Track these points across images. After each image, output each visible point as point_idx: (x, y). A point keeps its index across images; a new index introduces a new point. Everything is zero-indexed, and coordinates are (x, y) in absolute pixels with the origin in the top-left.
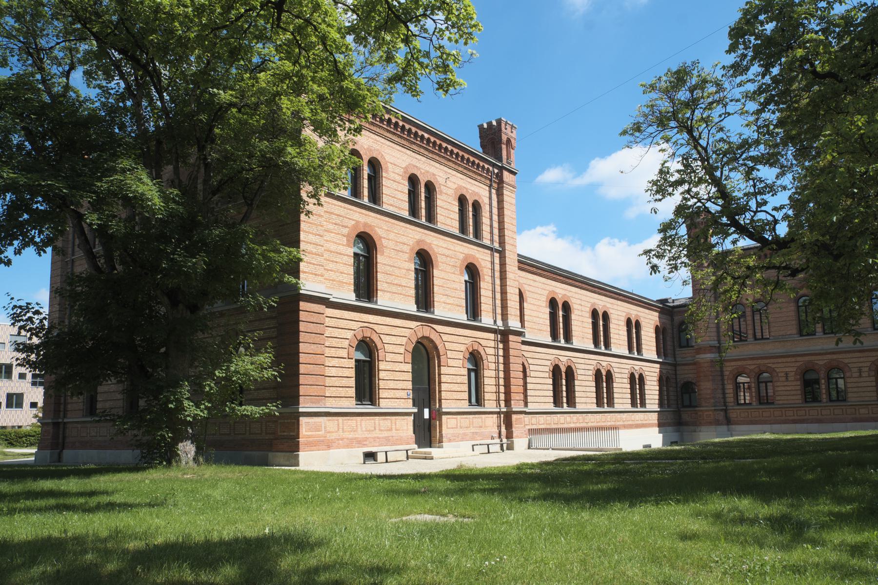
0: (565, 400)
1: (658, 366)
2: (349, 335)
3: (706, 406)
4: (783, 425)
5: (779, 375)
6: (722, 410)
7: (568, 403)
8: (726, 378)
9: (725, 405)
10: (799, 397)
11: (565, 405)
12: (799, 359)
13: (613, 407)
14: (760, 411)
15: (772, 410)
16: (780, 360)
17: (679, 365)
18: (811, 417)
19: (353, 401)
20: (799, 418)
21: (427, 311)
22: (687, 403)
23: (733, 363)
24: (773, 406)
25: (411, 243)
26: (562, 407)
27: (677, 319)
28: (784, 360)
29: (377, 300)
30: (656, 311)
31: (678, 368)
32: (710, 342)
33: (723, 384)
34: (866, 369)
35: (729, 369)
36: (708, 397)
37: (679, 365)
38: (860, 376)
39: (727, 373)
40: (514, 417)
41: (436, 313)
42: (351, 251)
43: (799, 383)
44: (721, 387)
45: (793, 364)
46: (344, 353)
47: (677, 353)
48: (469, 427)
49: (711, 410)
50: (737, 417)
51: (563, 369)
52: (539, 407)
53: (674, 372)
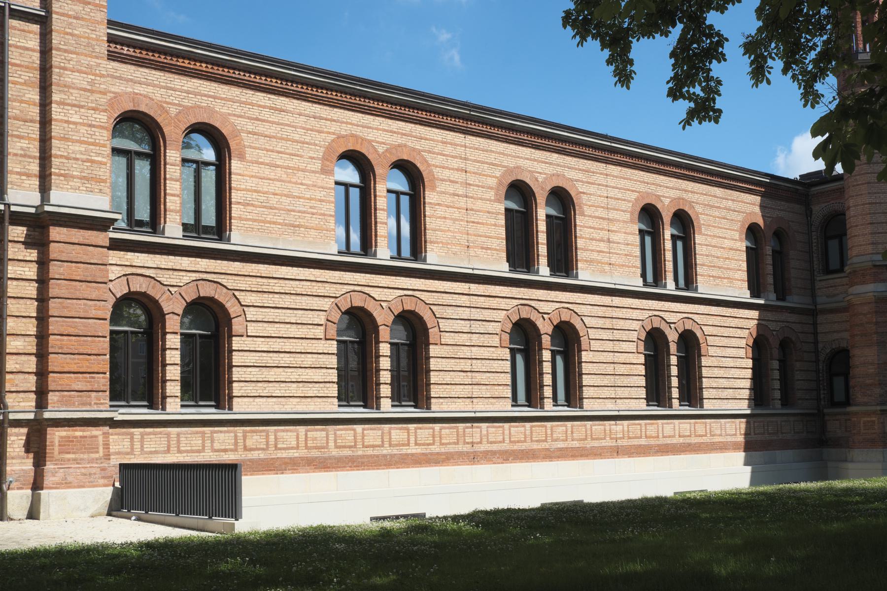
0: (675, 393)
1: (755, 314)
2: (501, 315)
3: (866, 404)
7: (681, 399)
11: (676, 403)
13: (702, 406)
17: (825, 311)
19: (105, 398)
21: (568, 275)
22: (839, 396)
25: (498, 174)
26: (671, 406)
27: (819, 210)
29: (577, 273)
30: (759, 196)
31: (821, 319)
36: (868, 382)
37: (825, 311)
40: (55, 436)
41: (379, 256)
42: (501, 208)
46: (319, 332)
47: (818, 285)
49: (874, 413)
51: (672, 336)
52: (277, 409)
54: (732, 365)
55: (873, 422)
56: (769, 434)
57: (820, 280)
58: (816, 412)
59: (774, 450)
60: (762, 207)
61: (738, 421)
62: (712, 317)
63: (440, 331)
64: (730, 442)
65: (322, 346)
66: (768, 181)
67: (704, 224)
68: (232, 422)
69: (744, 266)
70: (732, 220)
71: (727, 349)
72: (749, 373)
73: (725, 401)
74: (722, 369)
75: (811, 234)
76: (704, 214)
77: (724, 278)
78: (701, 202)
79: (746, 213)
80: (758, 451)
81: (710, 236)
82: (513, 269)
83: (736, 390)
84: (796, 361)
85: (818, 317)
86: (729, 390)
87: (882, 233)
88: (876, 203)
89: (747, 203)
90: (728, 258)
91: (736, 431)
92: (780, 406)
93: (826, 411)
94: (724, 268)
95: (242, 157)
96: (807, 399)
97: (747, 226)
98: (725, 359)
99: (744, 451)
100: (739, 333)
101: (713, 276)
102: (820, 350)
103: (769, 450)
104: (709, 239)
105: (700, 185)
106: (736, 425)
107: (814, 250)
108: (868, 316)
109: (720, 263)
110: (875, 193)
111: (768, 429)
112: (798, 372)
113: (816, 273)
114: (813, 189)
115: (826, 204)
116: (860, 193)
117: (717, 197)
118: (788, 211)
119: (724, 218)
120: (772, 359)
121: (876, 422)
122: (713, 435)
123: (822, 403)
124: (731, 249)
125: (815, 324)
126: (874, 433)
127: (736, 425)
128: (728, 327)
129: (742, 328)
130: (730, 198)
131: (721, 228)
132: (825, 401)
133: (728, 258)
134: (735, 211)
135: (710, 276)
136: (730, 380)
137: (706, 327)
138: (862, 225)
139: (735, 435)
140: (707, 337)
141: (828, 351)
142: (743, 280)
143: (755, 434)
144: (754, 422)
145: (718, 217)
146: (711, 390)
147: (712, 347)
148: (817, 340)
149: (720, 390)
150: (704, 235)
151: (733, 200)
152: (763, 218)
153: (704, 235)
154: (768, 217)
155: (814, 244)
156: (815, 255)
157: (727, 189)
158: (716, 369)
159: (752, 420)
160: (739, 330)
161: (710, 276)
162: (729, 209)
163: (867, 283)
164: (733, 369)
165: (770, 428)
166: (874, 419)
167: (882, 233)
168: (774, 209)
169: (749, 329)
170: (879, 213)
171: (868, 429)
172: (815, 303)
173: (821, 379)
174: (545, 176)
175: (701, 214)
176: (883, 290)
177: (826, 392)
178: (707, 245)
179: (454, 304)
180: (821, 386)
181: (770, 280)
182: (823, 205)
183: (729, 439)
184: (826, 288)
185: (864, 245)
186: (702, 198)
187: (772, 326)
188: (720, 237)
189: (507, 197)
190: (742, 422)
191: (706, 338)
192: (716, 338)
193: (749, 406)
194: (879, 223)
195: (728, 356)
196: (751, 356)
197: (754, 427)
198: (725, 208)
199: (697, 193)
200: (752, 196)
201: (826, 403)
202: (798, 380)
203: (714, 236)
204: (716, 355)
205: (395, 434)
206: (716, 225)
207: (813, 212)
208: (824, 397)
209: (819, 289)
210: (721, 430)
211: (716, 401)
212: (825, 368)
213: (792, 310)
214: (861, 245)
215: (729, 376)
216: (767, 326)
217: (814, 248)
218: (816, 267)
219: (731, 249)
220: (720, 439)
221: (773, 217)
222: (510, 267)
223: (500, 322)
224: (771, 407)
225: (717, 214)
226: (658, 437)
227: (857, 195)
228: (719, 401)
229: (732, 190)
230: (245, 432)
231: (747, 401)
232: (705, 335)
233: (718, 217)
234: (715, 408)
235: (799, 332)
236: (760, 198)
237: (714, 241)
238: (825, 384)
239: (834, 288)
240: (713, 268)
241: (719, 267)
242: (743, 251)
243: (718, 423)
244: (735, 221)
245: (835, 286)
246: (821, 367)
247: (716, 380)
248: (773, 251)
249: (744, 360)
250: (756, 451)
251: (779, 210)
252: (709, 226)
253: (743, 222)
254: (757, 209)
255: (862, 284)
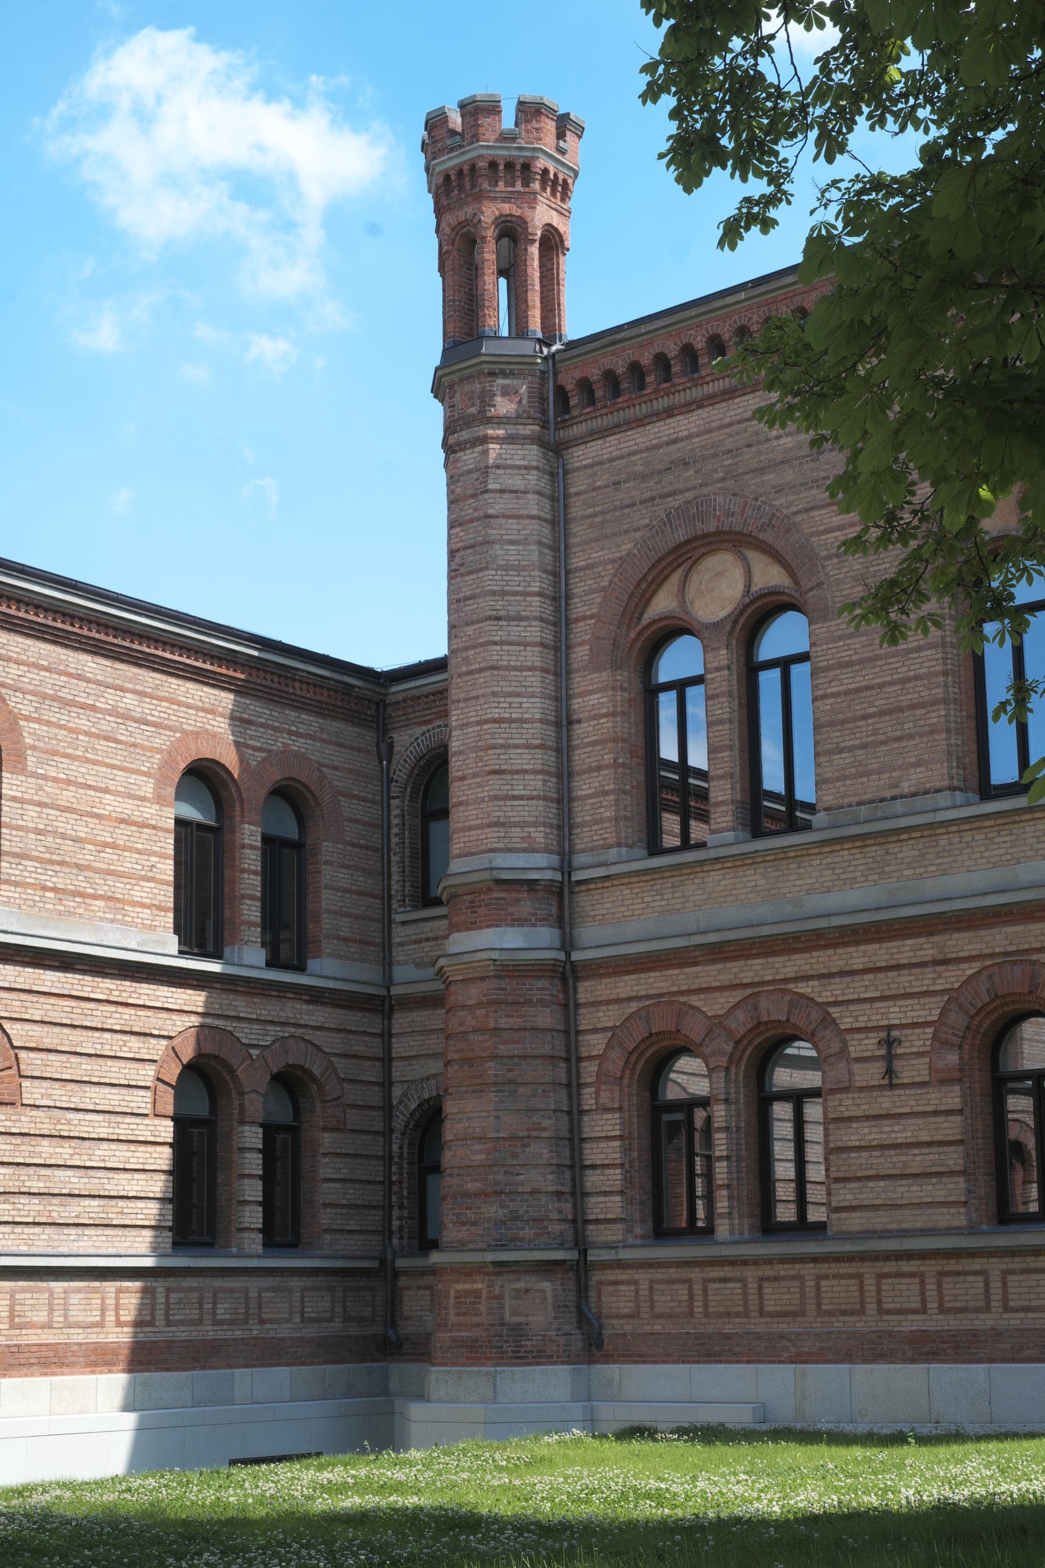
1: (195, 999)
4: (861, 1370)
5: (854, 1050)
6: (548, 1268)
8: (589, 1071)
9: (582, 1245)
10: (955, 1188)
12: (961, 943)
14: (751, 1274)
15: (809, 1270)
16: (858, 956)
18: (1015, 1320)
20: (953, 1323)
23: (627, 985)
24: (811, 1248)
28: (880, 953)
32: (502, 860)
33: (575, 1114)
34: (918, 1041)
35: (608, 1017)
36: (472, 1186)
38: (891, 1080)
39: (594, 1044)
43: (952, 1097)
44: (552, 1125)
45: (927, 979)
47: (399, 934)
48: (802, 1313)
50: (634, 1315)
53: (374, 1047)
54: (103, 1133)
55: (477, 1293)
56: (216, 1322)
57: (404, 923)
58: (375, 1264)
59: (231, 1367)
60: (237, 720)
61: (110, 1287)
62: (43, 999)
63: (21, 1076)
64: (80, 1344)
65: (145, 1129)
66: (256, 653)
67: (34, 748)
68: (65, 1272)
69: (167, 869)
70: (134, 745)
71: (87, 1088)
72: (163, 1157)
73: (73, 1231)
74: (66, 1143)
75: (389, 805)
76: (38, 721)
77: (95, 897)
78: (32, 687)
79: (183, 731)
80: (177, 1369)
81: (55, 780)
82: (187, 949)
83: (113, 1202)
84: (325, 1129)
85: (395, 1016)
86: (87, 1202)
87: (521, 798)
88: (510, 721)
89: (189, 706)
90: (114, 846)
91: (103, 1315)
92: (260, 1249)
93: (400, 1263)
94: (98, 871)
95: (21, 769)
96: (349, 1232)
97: (183, 766)
98: (80, 1116)
99: (129, 1371)
100: (134, 1046)
101: (54, 890)
102: (395, 1103)
103: (212, 1368)
104: (50, 788)
105: (29, 642)
106: (103, 1299)
107: (393, 845)
108: (478, 1012)
109: (86, 855)
110: (511, 695)
111: (214, 1309)
112: (326, 1160)
113: (395, 905)
114: (394, 689)
115: (424, 728)
116: (474, 693)
117: (88, 681)
118: (323, 741)
119: (107, 738)
120: (242, 1122)
121: (484, 1295)
122: (20, 1327)
123: (395, 1241)
124: (122, 821)
125: (387, 1036)
126: (477, 1325)
127: (103, 1299)
128: (96, 1029)
129: (145, 1035)
130: (131, 686)
131: (95, 763)
132: (401, 1238)
133: (114, 846)
134: (147, 723)
135: (45, 888)
136: (91, 1173)
137: (18, 1026)
138: (475, 775)
139: (101, 1324)
140: (22, 1054)
141: (413, 1107)
142: (160, 908)
143: (169, 1324)
144: (169, 1290)
145: (86, 733)
146: (24, 1200)
147: (36, 1083)
148: (390, 1077)
149: (55, 1201)
150: (34, 775)
151: (142, 694)
152: (238, 750)
153: (34, 775)
154: (254, 749)
155: (395, 831)
156: (395, 858)
157: (122, 661)
158: (45, 1142)
159: (160, 1285)
160: (133, 1038)
161: (45, 888)
162: (126, 716)
163: (481, 928)
164: (105, 1145)
165: (221, 1308)
166: (479, 1286)
167: (521, 798)
168: (275, 729)
169: (170, 1038)
170: (516, 747)
171: (465, 1314)
172: (388, 982)
173: (394, 1178)
174: (263, 755)
175: (28, 719)
176: (520, 945)
177: (405, 1213)
178: (40, 804)
179: (65, 1021)
180: (394, 1198)
181: (252, 911)
182: (419, 730)
183: (78, 1336)
184: (416, 942)
185: (478, 827)
186: (33, 677)
187: (246, 1034)
188: (90, 787)
189: (178, 797)
190: (127, 1290)
191: (16, 1055)
192: (52, 1057)
193: (156, 1250)
194: (517, 772)
195: (91, 1107)
196: (170, 1110)
197: (167, 1303)
198: (114, 712)
199: (18, 663)
200: (206, 689)
201: (405, 1242)
202: (327, 1180)
203: (69, 782)
204: (51, 1104)
205: (681, 1292)
206: (80, 753)
207: (396, 749)
208: (401, 1228)
209: (401, 944)
210: (51, 1311)
211: (38, 1230)
212: (405, 1151)
213: (315, 996)
214: (470, 829)
215: (88, 1164)
216: (231, 1033)
217: (395, 840)
218: (395, 887)
219: (122, 821)
220: (48, 1337)
221: (270, 751)
222: (180, 943)
223: (156, 1061)
224: (234, 1250)
225: (83, 723)
226: (691, 1314)
227: (465, 700)
228: (49, 1230)
229: (140, 666)
230: (119, 1291)
231: (148, 1234)
232: (13, 1047)
233: (86, 733)
234: (35, 1250)
235: (336, 1055)
236: (232, 696)
237: (68, 796)
238: (405, 1193)
239: (433, 943)
240: (57, 868)
241: (77, 866)
242: (167, 831)
243: (39, 1291)
244: (143, 748)
245: (435, 939)
246: (395, 1148)
247: (43, 1171)
248: (266, 839)
249: (146, 1121)
250: (167, 1370)
251: (290, 733)
252: (55, 753)
253: (169, 753)
254: (221, 726)
255: (467, 930)
